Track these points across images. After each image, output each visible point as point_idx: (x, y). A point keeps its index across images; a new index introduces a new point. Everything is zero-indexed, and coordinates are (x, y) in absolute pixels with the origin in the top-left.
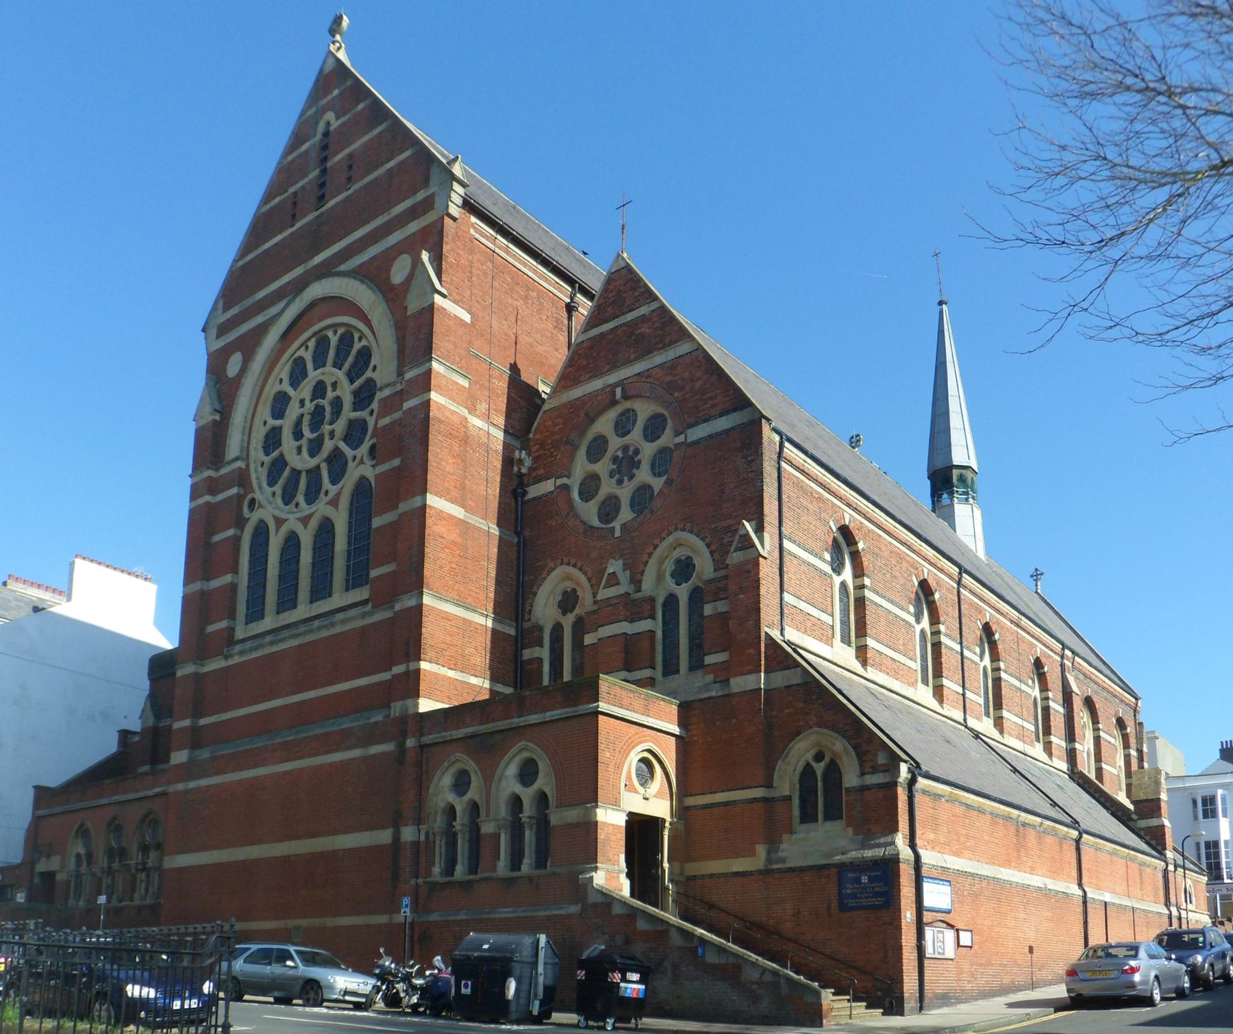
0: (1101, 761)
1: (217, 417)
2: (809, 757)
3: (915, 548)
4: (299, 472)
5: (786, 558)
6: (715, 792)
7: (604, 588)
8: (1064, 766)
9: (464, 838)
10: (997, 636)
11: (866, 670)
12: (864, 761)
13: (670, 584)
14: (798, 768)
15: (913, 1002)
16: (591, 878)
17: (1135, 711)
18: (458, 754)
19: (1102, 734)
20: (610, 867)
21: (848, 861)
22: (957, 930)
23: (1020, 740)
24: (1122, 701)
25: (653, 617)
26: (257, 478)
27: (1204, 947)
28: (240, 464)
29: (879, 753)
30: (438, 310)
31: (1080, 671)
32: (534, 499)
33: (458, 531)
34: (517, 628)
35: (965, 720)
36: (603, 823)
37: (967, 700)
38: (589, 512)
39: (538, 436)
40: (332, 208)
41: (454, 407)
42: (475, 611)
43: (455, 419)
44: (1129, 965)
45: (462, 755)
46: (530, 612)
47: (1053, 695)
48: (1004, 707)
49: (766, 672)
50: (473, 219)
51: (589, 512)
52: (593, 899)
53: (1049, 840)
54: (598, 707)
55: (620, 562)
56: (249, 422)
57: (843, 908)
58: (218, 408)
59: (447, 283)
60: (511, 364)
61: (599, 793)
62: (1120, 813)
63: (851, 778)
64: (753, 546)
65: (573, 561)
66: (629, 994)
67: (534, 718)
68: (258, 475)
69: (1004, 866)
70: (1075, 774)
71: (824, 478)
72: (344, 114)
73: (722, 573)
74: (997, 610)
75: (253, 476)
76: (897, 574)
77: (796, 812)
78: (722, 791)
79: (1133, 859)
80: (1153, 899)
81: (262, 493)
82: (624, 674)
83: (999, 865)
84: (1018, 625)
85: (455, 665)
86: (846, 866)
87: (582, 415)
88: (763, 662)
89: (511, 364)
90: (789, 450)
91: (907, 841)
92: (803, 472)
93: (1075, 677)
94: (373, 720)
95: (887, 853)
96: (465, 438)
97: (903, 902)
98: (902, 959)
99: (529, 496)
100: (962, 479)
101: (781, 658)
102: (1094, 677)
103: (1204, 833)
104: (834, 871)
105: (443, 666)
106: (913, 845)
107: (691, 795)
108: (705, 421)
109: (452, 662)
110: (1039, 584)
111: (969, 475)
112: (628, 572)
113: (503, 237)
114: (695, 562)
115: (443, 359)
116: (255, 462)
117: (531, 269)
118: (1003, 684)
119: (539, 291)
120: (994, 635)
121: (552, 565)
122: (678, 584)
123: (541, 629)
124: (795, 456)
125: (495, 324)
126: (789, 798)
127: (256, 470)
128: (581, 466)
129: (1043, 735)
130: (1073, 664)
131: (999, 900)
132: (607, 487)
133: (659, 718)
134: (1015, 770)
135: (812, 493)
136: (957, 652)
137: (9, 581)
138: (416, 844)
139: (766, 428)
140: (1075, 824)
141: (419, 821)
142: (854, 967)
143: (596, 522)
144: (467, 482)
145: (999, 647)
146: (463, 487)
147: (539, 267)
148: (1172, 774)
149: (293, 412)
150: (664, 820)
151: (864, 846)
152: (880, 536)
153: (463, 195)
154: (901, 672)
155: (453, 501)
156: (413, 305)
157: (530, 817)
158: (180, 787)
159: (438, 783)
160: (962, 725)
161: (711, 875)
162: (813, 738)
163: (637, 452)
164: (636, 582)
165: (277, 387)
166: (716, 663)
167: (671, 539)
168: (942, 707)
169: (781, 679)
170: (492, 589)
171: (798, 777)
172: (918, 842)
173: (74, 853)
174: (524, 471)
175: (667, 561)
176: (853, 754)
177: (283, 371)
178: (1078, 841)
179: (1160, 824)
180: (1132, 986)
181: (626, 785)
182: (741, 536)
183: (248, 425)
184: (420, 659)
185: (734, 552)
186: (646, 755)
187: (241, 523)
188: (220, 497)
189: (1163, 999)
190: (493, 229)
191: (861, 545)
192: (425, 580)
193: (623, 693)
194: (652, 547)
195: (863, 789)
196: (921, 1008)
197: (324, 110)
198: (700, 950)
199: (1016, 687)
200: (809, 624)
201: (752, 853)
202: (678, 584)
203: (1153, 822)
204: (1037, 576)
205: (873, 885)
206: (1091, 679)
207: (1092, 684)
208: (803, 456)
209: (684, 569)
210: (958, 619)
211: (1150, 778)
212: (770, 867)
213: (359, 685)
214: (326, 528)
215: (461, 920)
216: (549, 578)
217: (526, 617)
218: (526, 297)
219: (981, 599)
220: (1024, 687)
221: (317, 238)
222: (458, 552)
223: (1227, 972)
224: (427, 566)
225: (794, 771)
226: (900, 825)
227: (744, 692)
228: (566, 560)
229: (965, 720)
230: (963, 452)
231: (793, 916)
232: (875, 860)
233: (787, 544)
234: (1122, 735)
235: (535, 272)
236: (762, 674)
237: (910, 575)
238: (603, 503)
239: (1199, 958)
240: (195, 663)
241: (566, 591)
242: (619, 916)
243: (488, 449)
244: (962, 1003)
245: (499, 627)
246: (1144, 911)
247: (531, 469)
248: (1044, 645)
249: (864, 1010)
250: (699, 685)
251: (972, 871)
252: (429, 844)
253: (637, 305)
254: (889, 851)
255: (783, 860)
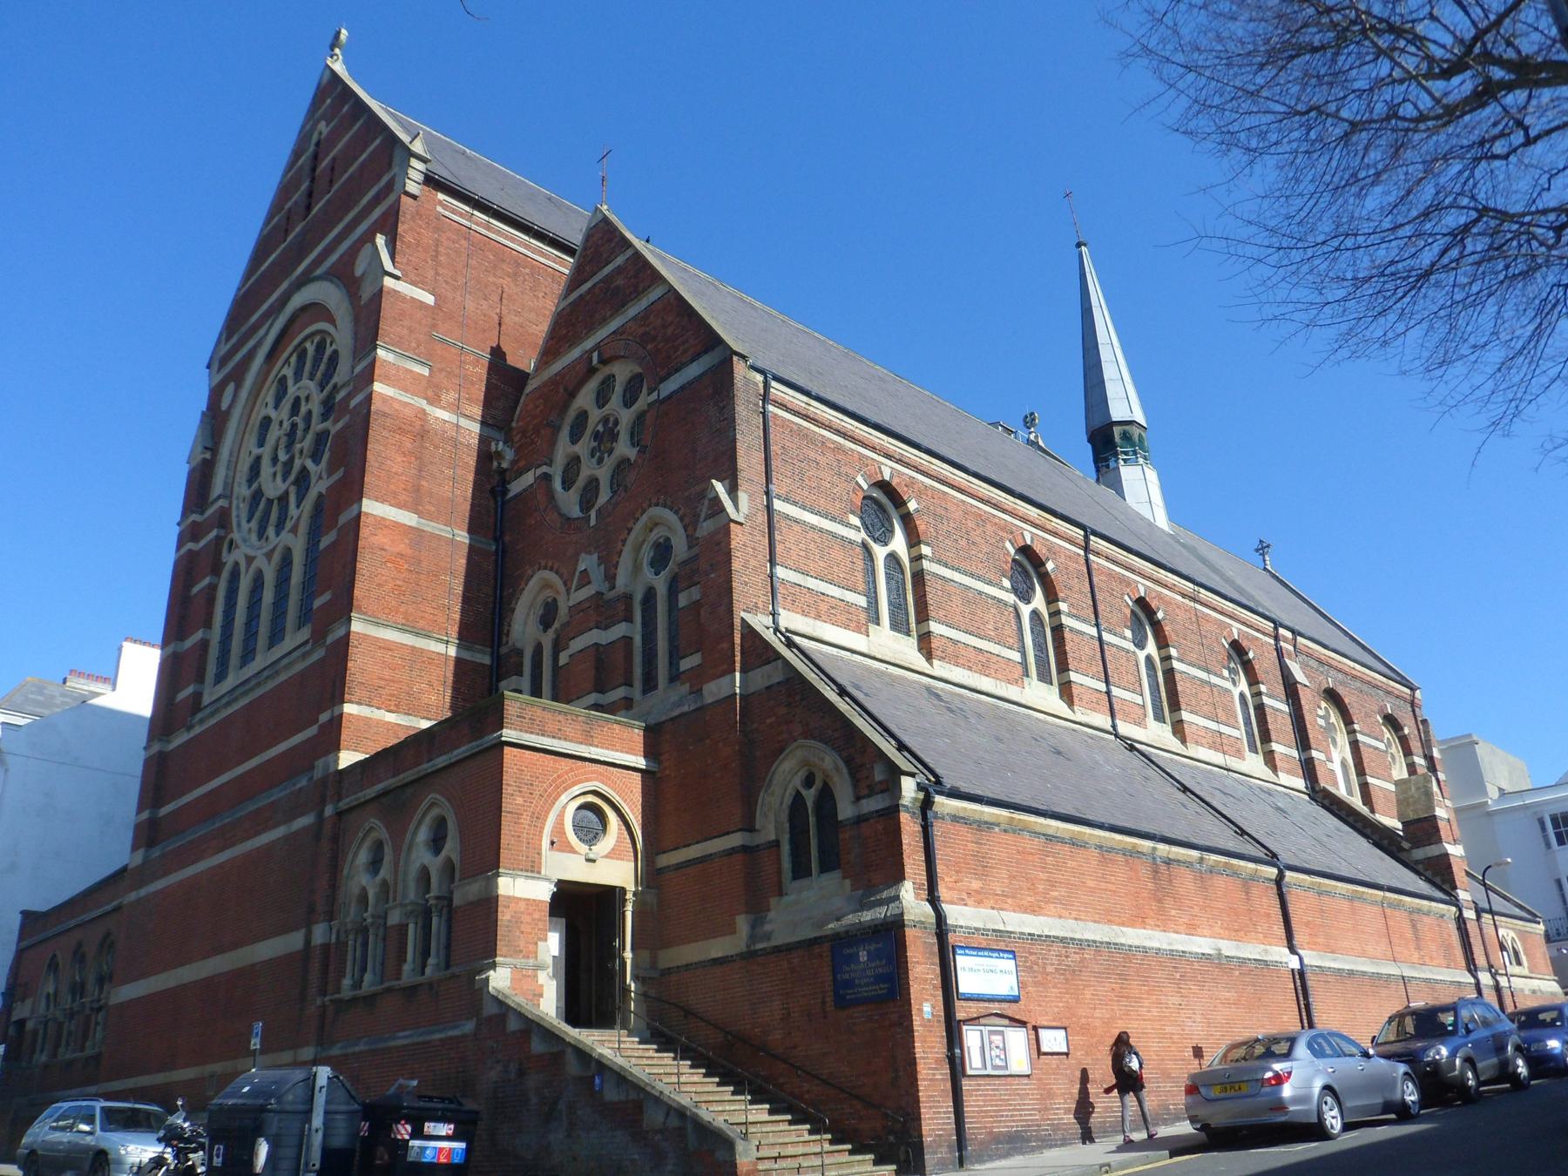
0: (1365, 774)
1: (208, 456)
2: (797, 782)
3: (1006, 507)
4: (273, 500)
5: (779, 523)
6: (689, 845)
7: (576, 590)
8: (1300, 783)
9: (377, 935)
10: (1160, 615)
11: (931, 664)
12: (857, 781)
13: (648, 573)
14: (786, 800)
15: (944, 1150)
16: (487, 979)
17: (1413, 704)
18: (372, 820)
19: (1360, 737)
20: (520, 962)
21: (844, 929)
22: (1035, 1028)
23: (1216, 750)
24: (1389, 693)
25: (629, 619)
26: (238, 516)
27: (1454, 1033)
28: (221, 503)
29: (875, 766)
30: (389, 293)
31: (1309, 655)
32: (516, 496)
33: (407, 542)
34: (492, 654)
35: (1114, 726)
36: (509, 897)
37: (1114, 700)
38: (569, 502)
39: (520, 424)
40: (317, 213)
41: (406, 398)
42: (429, 637)
43: (408, 412)
44: (1272, 1070)
45: (377, 822)
46: (508, 635)
47: (1268, 689)
48: (1183, 706)
49: (743, 671)
50: (441, 196)
51: (569, 502)
52: (490, 1010)
53: (1220, 882)
54: (501, 736)
55: (595, 556)
56: (235, 454)
57: (842, 1002)
58: (209, 446)
59: (402, 263)
60: (492, 348)
61: (501, 855)
62: (1386, 842)
63: (845, 810)
64: (723, 510)
65: (550, 564)
66: (429, 1157)
67: (441, 761)
68: (239, 510)
69: (1133, 926)
70: (1317, 792)
71: (843, 424)
72: (332, 121)
73: (695, 550)
74: (1157, 582)
75: (234, 514)
76: (978, 539)
77: (786, 864)
78: (697, 843)
79: (1396, 906)
80: (1443, 962)
81: (239, 531)
82: (593, 698)
83: (1123, 924)
84: (1194, 600)
85: (396, 705)
86: (841, 939)
87: (561, 390)
88: (738, 658)
89: (492, 348)
90: (777, 390)
91: (924, 894)
92: (806, 417)
93: (1301, 663)
94: (298, 786)
95: (888, 914)
96: (422, 432)
97: (915, 989)
98: (916, 1080)
99: (511, 494)
100: (1126, 437)
101: (758, 650)
102: (1333, 662)
103: (1509, 860)
104: (827, 946)
105: (378, 708)
106: (933, 900)
107: (664, 852)
108: (677, 371)
109: (393, 703)
110: (1267, 558)
111: (1135, 432)
112: (602, 567)
113: (483, 213)
114: (673, 542)
115: (393, 345)
116: (238, 498)
117: (521, 244)
118: (1178, 677)
119: (533, 266)
120: (1155, 613)
121: (530, 572)
122: (657, 574)
123: (519, 653)
124: (791, 399)
125: (470, 304)
126: (776, 844)
127: (238, 508)
128: (564, 448)
129: (1262, 743)
130: (1295, 646)
131: (1123, 977)
132: (587, 470)
133: (612, 747)
134: (1185, 789)
135: (824, 442)
136: (1092, 637)
137: (69, 677)
138: (326, 947)
139: (739, 368)
140: (1272, 858)
141: (330, 916)
142: (857, 1097)
143: (576, 512)
144: (424, 483)
145: (1166, 628)
146: (417, 489)
147: (532, 240)
148: (1508, 788)
149: (274, 433)
150: (623, 890)
151: (864, 906)
152: (945, 493)
153: (424, 171)
154: (992, 665)
155: (400, 506)
156: (366, 293)
157: (437, 898)
158: (133, 896)
159: (353, 861)
160: (1111, 734)
161: (687, 965)
162: (799, 753)
163: (616, 423)
164: (610, 578)
165: (263, 413)
166: (692, 668)
167: (644, 518)
168: (1073, 711)
169: (764, 677)
170: (458, 608)
171: (787, 812)
172: (943, 891)
173: (45, 993)
174: (505, 465)
175: (645, 546)
176: (845, 771)
177: (269, 395)
178: (1279, 881)
179: (1442, 852)
180: (1280, 1106)
181: (552, 843)
182: (710, 500)
183: (234, 459)
184: (343, 702)
185: (705, 520)
186: (591, 798)
187: (216, 569)
188: (203, 543)
189: (1347, 1127)
190: (468, 205)
191: (912, 506)
192: (355, 603)
193: (547, 715)
194: (626, 531)
195: (860, 820)
196: (961, 1164)
197: (318, 122)
198: (597, 1081)
199: (1201, 680)
200: (824, 607)
201: (731, 930)
202: (657, 574)
203: (1432, 851)
204: (1262, 549)
205: (874, 965)
206: (1330, 666)
207: (1333, 672)
208: (805, 398)
209: (662, 552)
210: (1089, 595)
211: (1418, 789)
212: (752, 948)
213: (294, 744)
214: (287, 561)
215: (360, 1052)
216: (527, 589)
217: (504, 639)
218: (515, 274)
219: (1127, 568)
220: (1214, 680)
221: (301, 249)
222: (406, 566)
223: (1511, 1069)
224: (358, 585)
225: (781, 804)
226: (908, 870)
227: (717, 701)
228: (543, 563)
229: (1114, 726)
230: (1124, 403)
231: (782, 1019)
232: (876, 926)
233: (778, 505)
234: (1399, 738)
235: (527, 247)
236: (738, 675)
237: (1002, 540)
238: (585, 489)
239: (1444, 1051)
240: (160, 740)
241: (548, 603)
242: (514, 1033)
243: (455, 443)
244: (1056, 1146)
245: (467, 656)
246: (1426, 980)
247: (514, 462)
248: (1244, 623)
249: (870, 1167)
250: (669, 700)
251: (1061, 934)
252: (341, 945)
253: (613, 257)
254: (892, 909)
255: (768, 937)
